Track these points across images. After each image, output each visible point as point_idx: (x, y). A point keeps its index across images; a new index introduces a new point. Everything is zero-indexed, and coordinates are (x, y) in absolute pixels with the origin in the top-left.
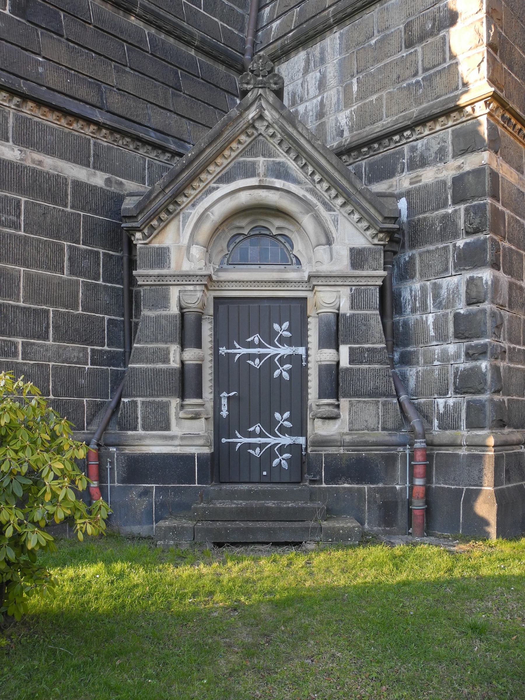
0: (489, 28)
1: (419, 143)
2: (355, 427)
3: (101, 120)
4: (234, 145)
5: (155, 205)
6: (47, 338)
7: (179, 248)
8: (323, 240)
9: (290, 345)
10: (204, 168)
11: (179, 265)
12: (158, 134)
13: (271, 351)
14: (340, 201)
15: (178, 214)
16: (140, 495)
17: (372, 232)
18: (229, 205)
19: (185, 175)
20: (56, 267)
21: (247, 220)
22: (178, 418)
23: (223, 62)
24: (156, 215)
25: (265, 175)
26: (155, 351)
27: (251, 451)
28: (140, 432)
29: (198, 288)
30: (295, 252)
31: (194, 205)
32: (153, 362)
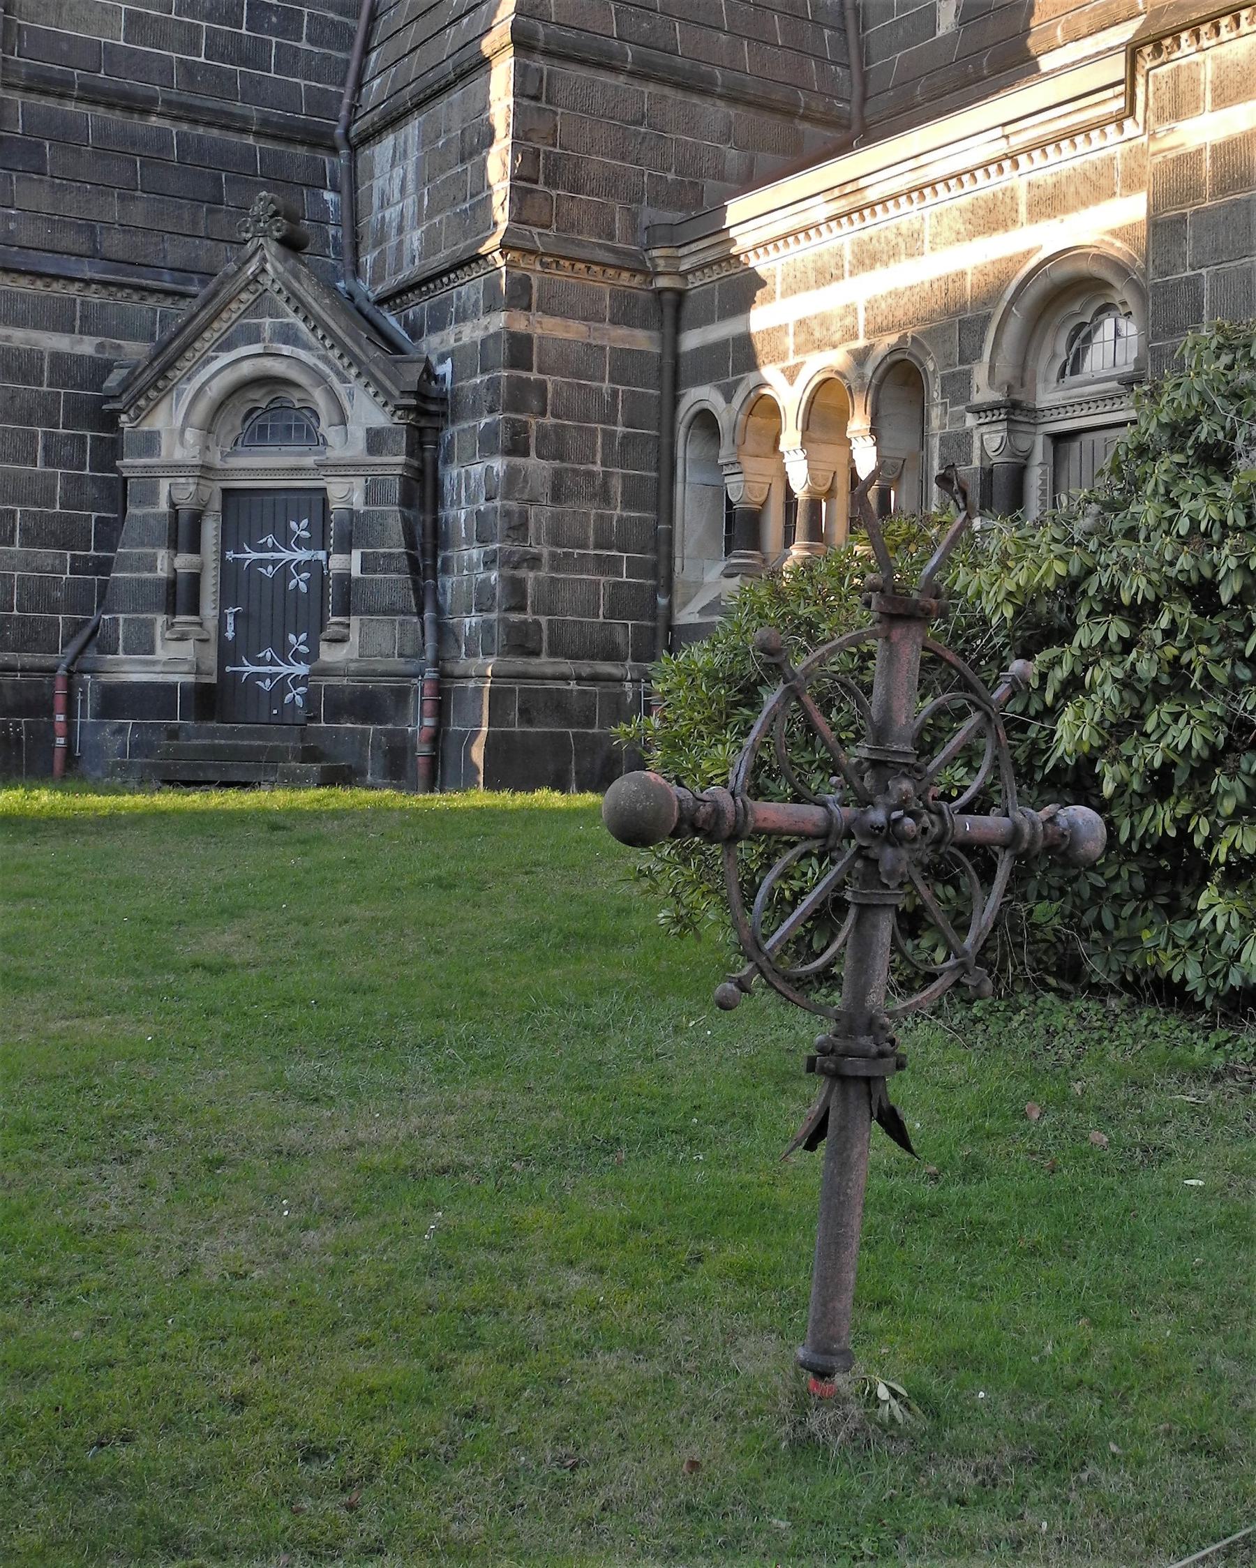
0: (514, 158)
1: (463, 289)
2: (367, 652)
3: (88, 275)
4: (233, 306)
5: (140, 383)
6: (12, 543)
7: (171, 431)
8: (336, 419)
9: (309, 549)
10: (197, 336)
11: (170, 454)
12: (177, 274)
13: (286, 555)
14: (354, 371)
15: (171, 390)
16: (114, 733)
17: (389, 408)
18: (230, 377)
19: (175, 344)
20: (26, 459)
21: (263, 391)
22: (165, 640)
23: (302, 143)
24: (142, 393)
25: (271, 341)
26: (140, 558)
27: (259, 683)
28: (121, 656)
29: (191, 480)
30: (320, 430)
31: (189, 379)
32: (138, 570)
